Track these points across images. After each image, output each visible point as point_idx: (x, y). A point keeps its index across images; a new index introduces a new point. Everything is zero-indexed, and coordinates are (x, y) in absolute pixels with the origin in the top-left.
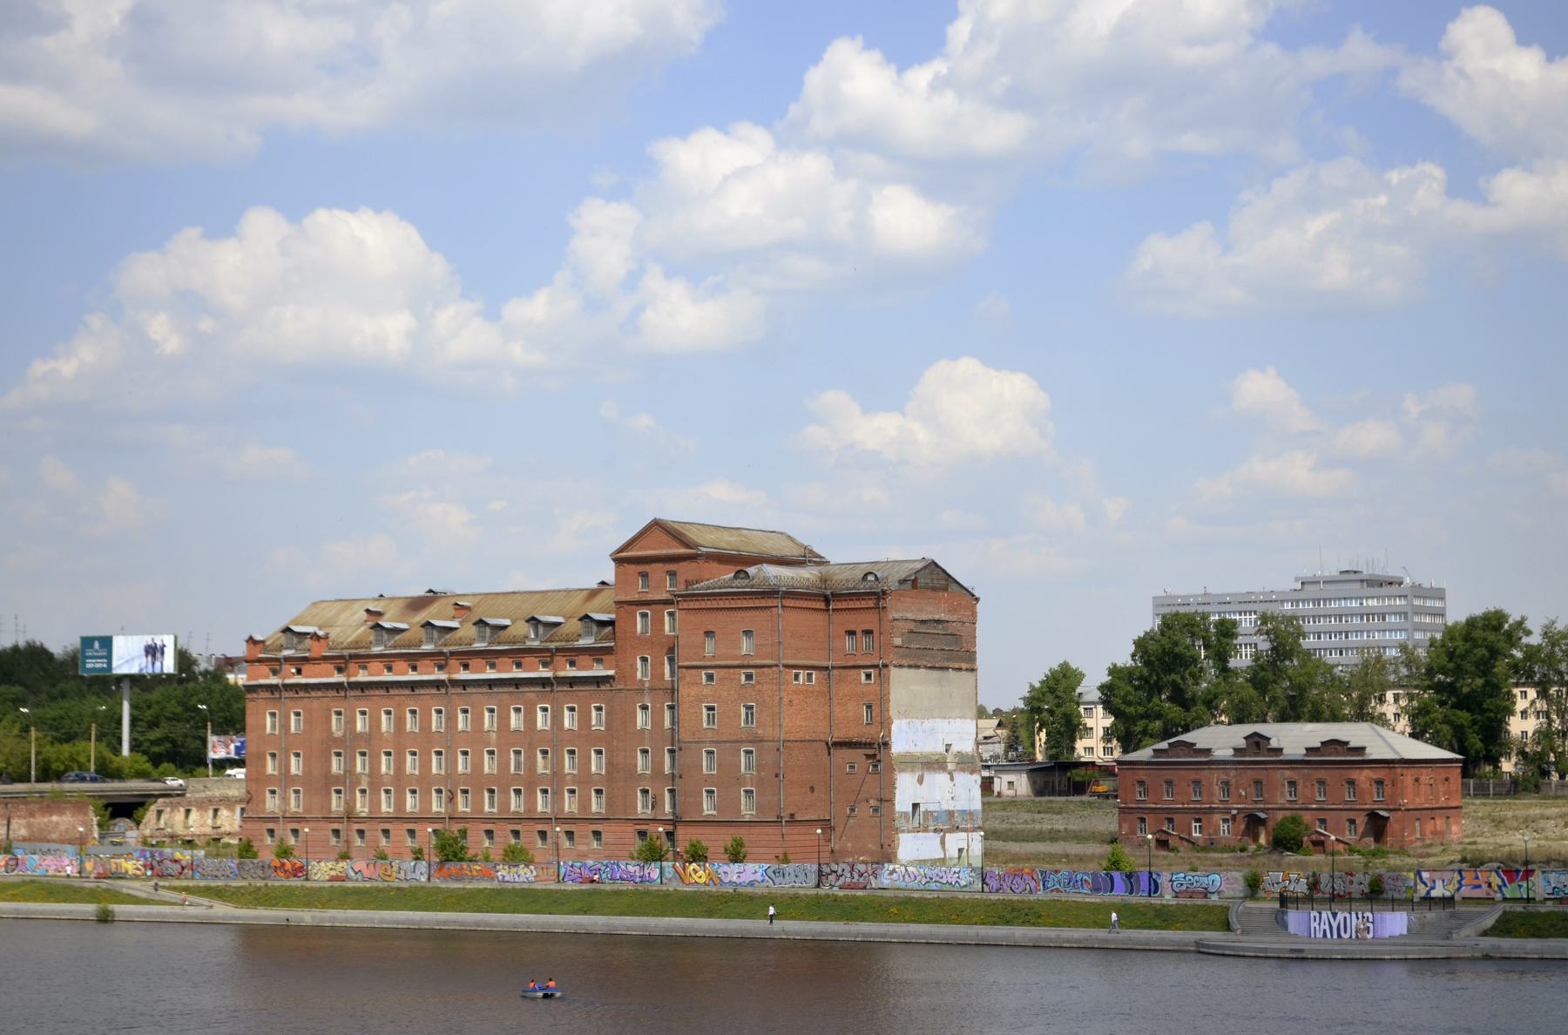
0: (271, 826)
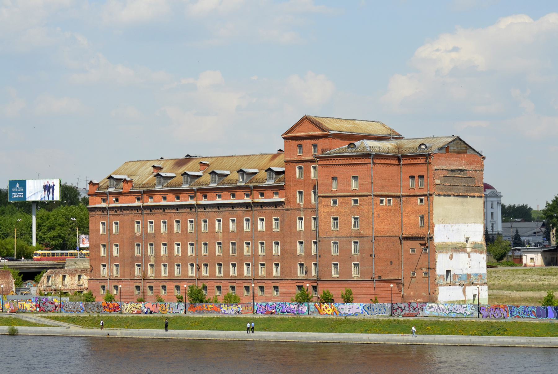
0: (103, 284)
